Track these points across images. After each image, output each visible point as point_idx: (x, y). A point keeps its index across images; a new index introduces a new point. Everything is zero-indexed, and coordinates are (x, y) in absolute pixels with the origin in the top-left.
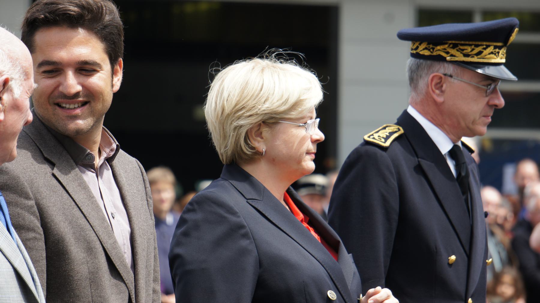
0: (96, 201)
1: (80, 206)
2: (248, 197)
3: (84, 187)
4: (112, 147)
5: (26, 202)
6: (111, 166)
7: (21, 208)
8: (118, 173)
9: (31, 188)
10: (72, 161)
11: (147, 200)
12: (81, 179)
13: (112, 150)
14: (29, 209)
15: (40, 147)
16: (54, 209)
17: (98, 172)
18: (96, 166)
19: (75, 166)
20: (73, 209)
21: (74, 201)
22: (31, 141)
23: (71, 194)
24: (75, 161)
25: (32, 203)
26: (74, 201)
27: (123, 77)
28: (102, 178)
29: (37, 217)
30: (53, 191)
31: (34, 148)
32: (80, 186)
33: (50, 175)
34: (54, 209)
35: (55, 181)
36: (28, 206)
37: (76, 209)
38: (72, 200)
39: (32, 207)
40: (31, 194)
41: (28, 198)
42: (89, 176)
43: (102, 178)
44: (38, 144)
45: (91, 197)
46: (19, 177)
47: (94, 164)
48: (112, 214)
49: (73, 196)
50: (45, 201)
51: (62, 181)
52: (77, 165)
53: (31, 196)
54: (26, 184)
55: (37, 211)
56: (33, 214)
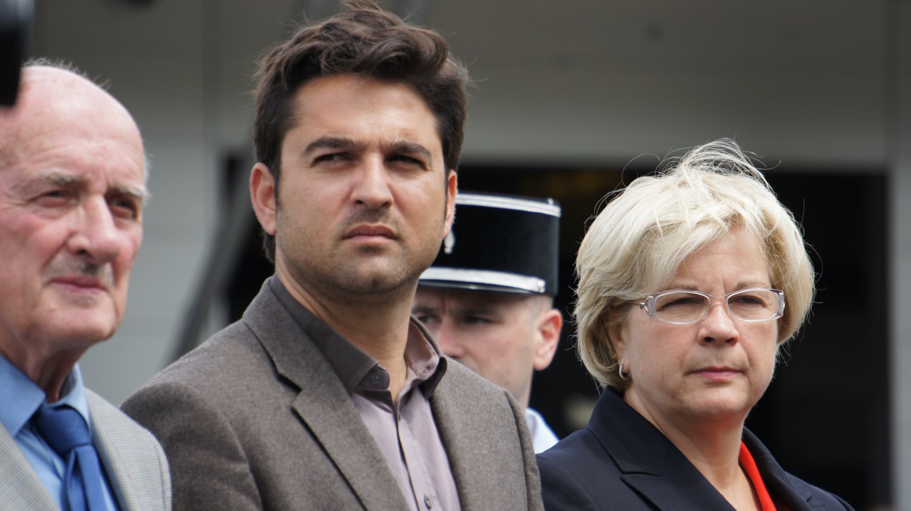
0: (386, 469)
1: (347, 476)
2: (625, 469)
3: (362, 438)
4: (429, 362)
5: (232, 466)
6: (432, 402)
7: (221, 480)
8: (444, 412)
9: (242, 437)
10: (339, 384)
11: (526, 476)
12: (357, 421)
13: (429, 368)
14: (237, 482)
15: (272, 354)
16: (291, 482)
17: (399, 409)
18: (393, 397)
19: (345, 395)
20: (334, 482)
21: (336, 466)
22: (255, 342)
23: (329, 451)
24: (346, 385)
25: (243, 467)
26: (336, 466)
27: (456, 215)
28: (409, 421)
29: (254, 499)
30: (291, 445)
31: (258, 356)
32: (353, 435)
33: (285, 410)
34: (291, 482)
35: (296, 426)
36: (235, 474)
37: (339, 483)
38: (331, 465)
39: (243, 476)
40: (240, 449)
41: (234, 457)
42: (378, 421)
43: (409, 421)
44: (268, 348)
45: (375, 461)
46: (215, 415)
47: (389, 394)
48: (426, 499)
49: (333, 456)
50: (271, 463)
51: (310, 424)
52: (350, 394)
53: (242, 453)
54: (230, 428)
55: (254, 486)
56: (245, 490)
